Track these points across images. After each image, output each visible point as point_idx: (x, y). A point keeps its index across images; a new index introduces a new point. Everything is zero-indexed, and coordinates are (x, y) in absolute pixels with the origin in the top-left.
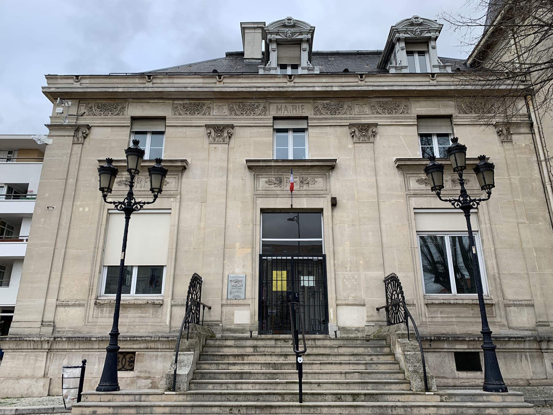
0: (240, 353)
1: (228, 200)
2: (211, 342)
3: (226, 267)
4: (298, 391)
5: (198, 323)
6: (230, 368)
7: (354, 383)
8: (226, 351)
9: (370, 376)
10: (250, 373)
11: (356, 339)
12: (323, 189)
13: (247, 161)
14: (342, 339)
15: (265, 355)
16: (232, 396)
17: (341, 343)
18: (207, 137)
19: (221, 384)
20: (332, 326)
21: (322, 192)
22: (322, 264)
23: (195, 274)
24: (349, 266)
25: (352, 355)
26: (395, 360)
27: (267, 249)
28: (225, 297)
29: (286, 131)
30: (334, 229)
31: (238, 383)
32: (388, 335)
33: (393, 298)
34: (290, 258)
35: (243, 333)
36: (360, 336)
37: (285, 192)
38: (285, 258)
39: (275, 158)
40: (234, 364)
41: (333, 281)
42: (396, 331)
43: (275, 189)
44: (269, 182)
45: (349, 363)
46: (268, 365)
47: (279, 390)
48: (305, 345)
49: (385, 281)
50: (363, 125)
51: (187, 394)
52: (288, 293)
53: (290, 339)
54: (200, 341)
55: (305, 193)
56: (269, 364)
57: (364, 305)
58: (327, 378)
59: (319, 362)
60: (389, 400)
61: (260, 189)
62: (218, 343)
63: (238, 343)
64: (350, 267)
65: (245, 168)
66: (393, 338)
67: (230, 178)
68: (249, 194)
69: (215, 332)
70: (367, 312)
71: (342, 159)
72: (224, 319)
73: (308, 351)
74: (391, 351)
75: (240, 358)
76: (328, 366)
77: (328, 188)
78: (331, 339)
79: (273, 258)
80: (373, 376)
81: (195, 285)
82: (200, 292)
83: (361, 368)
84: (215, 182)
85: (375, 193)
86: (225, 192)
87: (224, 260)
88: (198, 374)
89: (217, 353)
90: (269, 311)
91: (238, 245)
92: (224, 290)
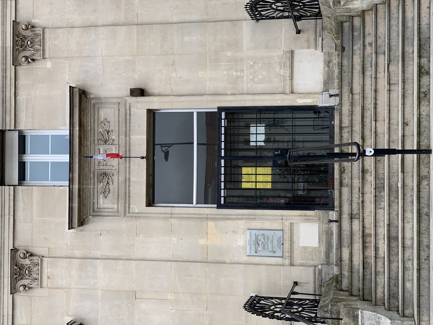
0: (361, 240)
1: (133, 257)
2: (345, 283)
3: (236, 259)
4: (415, 155)
5: (317, 302)
6: (382, 255)
7: (403, 72)
8: (357, 260)
9: (393, 48)
10: (389, 225)
11: (341, 66)
12: (116, 108)
13: (71, 227)
14: (341, 87)
15: (363, 202)
16: (422, 253)
17: (346, 89)
18: (30, 291)
19: (404, 269)
20: (323, 101)
21: (122, 110)
22: (232, 113)
23: (245, 307)
24: (234, 73)
25: (363, 73)
26: (371, 10)
27: (210, 196)
28: (280, 261)
29: (22, 166)
30: (179, 93)
31: (403, 243)
32: (336, 18)
33: (282, 8)
34: (223, 161)
35: (332, 234)
36: (337, 60)
37: (122, 167)
38: (223, 169)
39: (67, 183)
40: (376, 249)
41: (257, 97)
42: (330, 7)
43: (116, 184)
44: (106, 192)
45: (376, 78)
46: (378, 199)
47: (412, 182)
48: (349, 144)
49: (258, 20)
50: (15, 43)
51: (420, 320)
52: (275, 166)
53: (340, 165)
54: (342, 300)
55: (122, 137)
56: (375, 196)
57: (292, 52)
58: (396, 112)
59: (373, 123)
60: (428, 22)
61: (116, 206)
62: (346, 273)
63: (346, 241)
64: (237, 71)
65: (81, 231)
66: (339, 11)
67: (98, 254)
68: (123, 224)
69: (331, 276)
70: (303, 48)
71: (70, 77)
72: (311, 263)
73: (357, 139)
74: (358, 16)
75: (368, 240)
76: (379, 109)
77: (115, 100)
78: (341, 104)
79: (223, 187)
80: (393, 43)
81: (262, 308)
82: (272, 298)
83: (382, 60)
84: (104, 277)
85: (124, 28)
86: (121, 262)
87: (225, 263)
88: (391, 303)
89: (361, 274)
90: (301, 193)
91: (202, 242)
92: (269, 262)
